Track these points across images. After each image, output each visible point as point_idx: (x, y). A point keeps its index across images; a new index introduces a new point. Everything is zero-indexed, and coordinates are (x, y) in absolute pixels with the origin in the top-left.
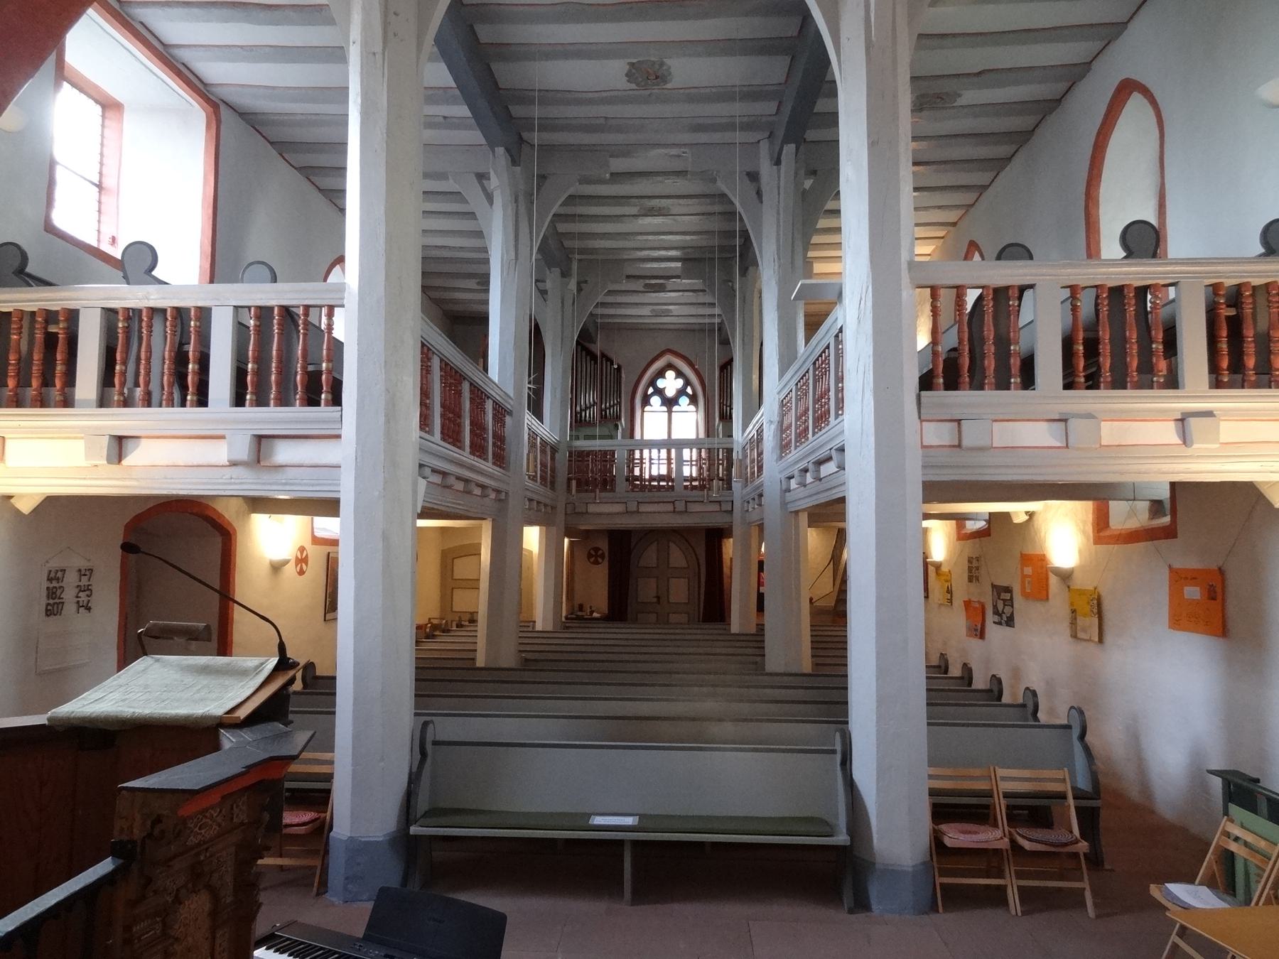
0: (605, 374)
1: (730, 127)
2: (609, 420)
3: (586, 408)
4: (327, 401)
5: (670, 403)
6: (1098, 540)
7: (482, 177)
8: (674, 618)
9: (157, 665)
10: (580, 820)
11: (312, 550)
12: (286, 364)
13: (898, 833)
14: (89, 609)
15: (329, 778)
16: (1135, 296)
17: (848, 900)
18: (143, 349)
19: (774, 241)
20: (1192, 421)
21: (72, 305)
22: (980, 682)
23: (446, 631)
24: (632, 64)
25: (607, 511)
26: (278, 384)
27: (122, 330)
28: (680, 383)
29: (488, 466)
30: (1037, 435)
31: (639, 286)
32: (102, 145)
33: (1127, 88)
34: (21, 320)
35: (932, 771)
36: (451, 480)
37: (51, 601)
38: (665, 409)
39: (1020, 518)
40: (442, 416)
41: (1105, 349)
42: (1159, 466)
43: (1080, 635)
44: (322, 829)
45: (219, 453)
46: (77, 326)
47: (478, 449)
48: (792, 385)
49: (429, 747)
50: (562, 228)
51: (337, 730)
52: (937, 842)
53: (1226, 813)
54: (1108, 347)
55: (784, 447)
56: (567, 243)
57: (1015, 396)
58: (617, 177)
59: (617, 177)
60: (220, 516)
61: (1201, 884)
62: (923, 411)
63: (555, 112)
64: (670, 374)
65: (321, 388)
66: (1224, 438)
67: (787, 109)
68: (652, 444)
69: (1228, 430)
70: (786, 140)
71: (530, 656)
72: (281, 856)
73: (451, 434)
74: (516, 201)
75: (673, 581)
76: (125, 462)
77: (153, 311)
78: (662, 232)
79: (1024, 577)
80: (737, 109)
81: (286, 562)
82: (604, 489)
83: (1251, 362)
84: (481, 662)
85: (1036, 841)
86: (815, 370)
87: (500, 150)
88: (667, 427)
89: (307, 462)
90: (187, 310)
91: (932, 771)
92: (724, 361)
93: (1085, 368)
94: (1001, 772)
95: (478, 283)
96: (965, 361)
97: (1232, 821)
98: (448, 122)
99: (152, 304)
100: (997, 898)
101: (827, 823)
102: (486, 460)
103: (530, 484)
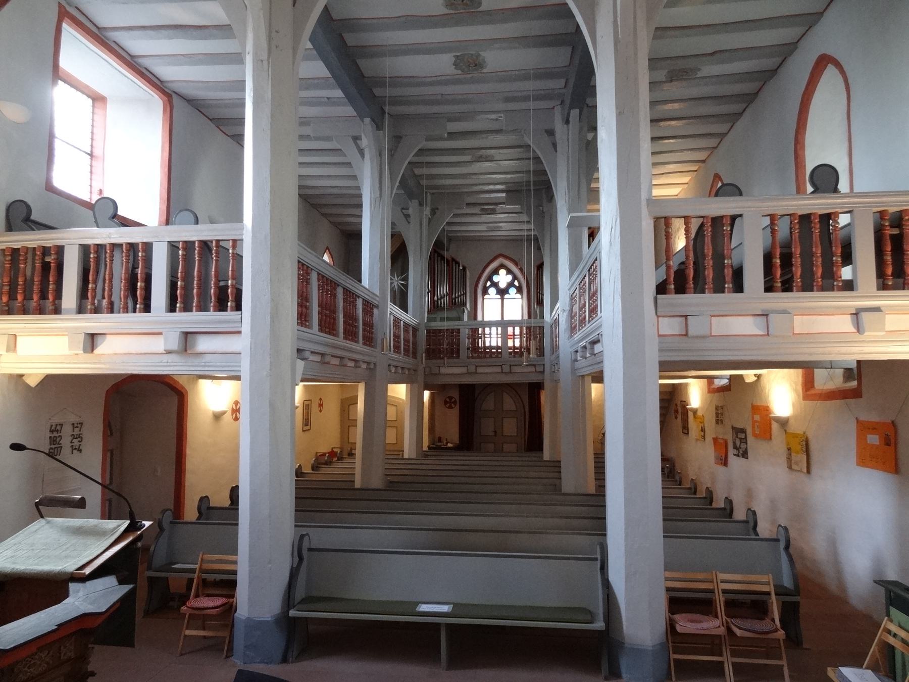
0: (454, 271)
1: (526, 99)
2: (457, 305)
4: (231, 307)
5: (502, 292)
7: (356, 139)
9: (47, 526)
10: (410, 607)
12: (206, 281)
13: (642, 620)
14: (80, 451)
15: (235, 573)
17: (605, 666)
18: (107, 273)
19: (565, 179)
20: (864, 316)
21: (59, 243)
22: (719, 503)
23: (340, 458)
25: (454, 372)
26: (199, 295)
27: (93, 259)
28: (509, 278)
29: (359, 346)
30: (745, 326)
31: (477, 210)
32: (93, 126)
33: (824, 61)
34: (26, 253)
35: (668, 574)
36: (327, 359)
37: (53, 446)
38: (499, 296)
40: (320, 313)
41: (797, 261)
42: (838, 349)
43: (794, 467)
44: (230, 609)
45: (158, 345)
46: (63, 256)
47: (351, 334)
48: (576, 285)
49: (305, 553)
50: (417, 171)
51: (240, 541)
52: (671, 626)
53: (888, 615)
54: (799, 260)
55: (573, 329)
57: (728, 298)
58: (452, 135)
59: (452, 135)
61: (867, 668)
63: (398, 92)
64: (503, 272)
65: (227, 298)
66: (888, 327)
67: (572, 81)
68: (491, 324)
69: (892, 322)
70: (571, 107)
71: (396, 479)
72: (204, 629)
73: (328, 326)
74: (380, 155)
76: (96, 352)
77: (114, 246)
78: (495, 171)
79: (754, 422)
80: (531, 86)
81: (224, 413)
82: (451, 357)
84: (358, 485)
85: (745, 630)
86: (590, 275)
87: (367, 120)
88: (500, 310)
89: (220, 350)
90: (137, 244)
91: (668, 574)
92: (538, 263)
93: (782, 275)
94: (723, 576)
97: (891, 621)
99: (113, 241)
101: (590, 613)
102: (357, 342)
103: (395, 356)
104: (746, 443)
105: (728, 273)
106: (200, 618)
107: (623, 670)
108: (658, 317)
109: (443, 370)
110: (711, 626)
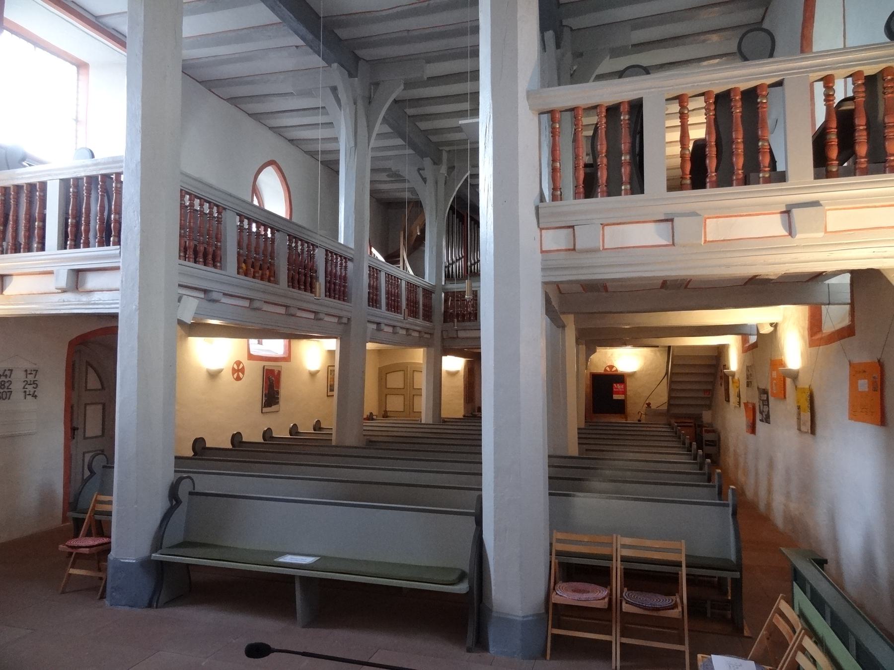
3: (453, 262)
11: (246, 362)
13: (517, 585)
14: (36, 397)
15: (109, 514)
16: (742, 99)
30: (646, 235)
44: (105, 549)
47: (413, 313)
56: (434, 139)
57: (625, 201)
65: (109, 233)
69: (835, 219)
71: (374, 439)
74: (355, 103)
83: (862, 150)
87: (335, 65)
89: (105, 287)
95: (388, 176)
100: (602, 651)
104: (768, 405)
106: (79, 559)
107: (491, 643)
108: (541, 229)
109: (462, 334)
110: (594, 596)
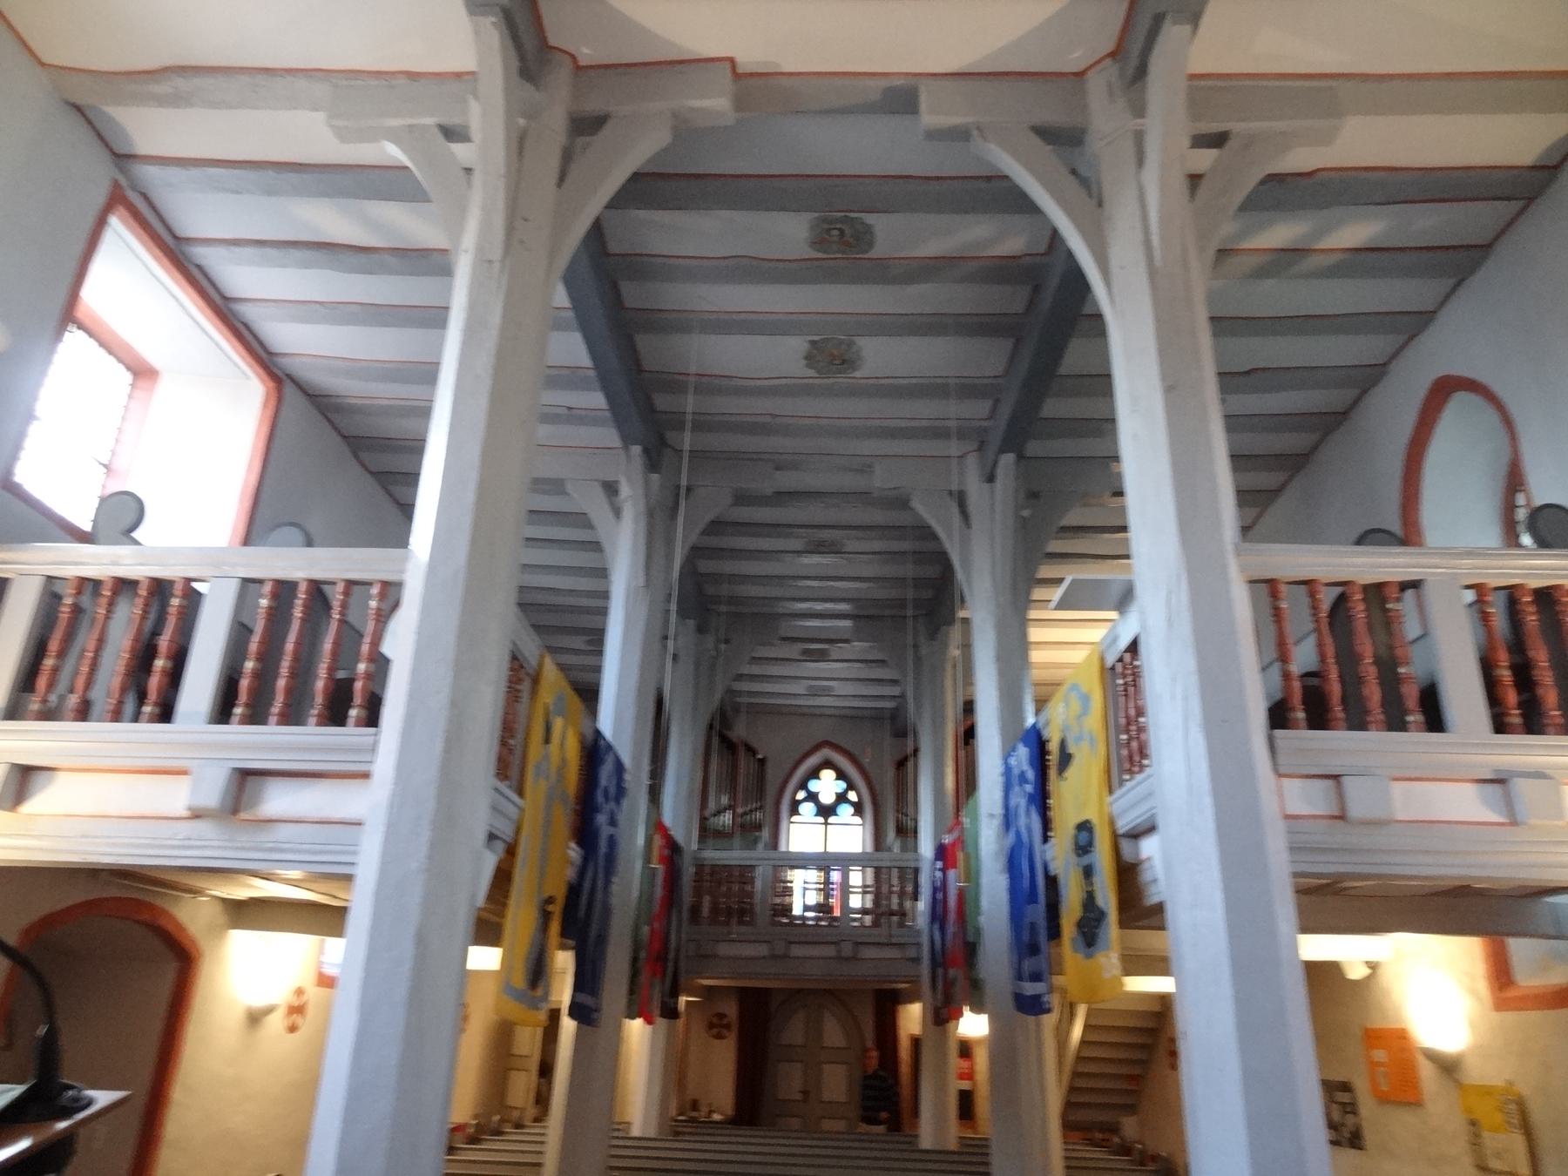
5: (826, 812)
6: (1501, 1004)
8: (827, 1125)
12: (304, 666)
24: (813, 343)
25: (741, 956)
26: (289, 691)
30: (1462, 803)
31: (793, 651)
33: (1444, 389)
38: (821, 820)
39: (1356, 972)
50: (705, 566)
56: (710, 590)
57: (1415, 743)
58: (782, 497)
60: (180, 927)
62: (1281, 759)
64: (828, 775)
65: (350, 701)
67: (1005, 411)
70: (1003, 450)
75: (827, 1068)
76: (28, 808)
81: (269, 1010)
82: (741, 922)
87: (636, 450)
88: (823, 840)
92: (899, 757)
95: (589, 642)
96: (1335, 689)
98: (572, 416)
105: (1411, 694)
